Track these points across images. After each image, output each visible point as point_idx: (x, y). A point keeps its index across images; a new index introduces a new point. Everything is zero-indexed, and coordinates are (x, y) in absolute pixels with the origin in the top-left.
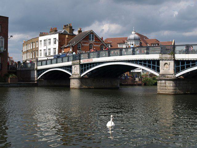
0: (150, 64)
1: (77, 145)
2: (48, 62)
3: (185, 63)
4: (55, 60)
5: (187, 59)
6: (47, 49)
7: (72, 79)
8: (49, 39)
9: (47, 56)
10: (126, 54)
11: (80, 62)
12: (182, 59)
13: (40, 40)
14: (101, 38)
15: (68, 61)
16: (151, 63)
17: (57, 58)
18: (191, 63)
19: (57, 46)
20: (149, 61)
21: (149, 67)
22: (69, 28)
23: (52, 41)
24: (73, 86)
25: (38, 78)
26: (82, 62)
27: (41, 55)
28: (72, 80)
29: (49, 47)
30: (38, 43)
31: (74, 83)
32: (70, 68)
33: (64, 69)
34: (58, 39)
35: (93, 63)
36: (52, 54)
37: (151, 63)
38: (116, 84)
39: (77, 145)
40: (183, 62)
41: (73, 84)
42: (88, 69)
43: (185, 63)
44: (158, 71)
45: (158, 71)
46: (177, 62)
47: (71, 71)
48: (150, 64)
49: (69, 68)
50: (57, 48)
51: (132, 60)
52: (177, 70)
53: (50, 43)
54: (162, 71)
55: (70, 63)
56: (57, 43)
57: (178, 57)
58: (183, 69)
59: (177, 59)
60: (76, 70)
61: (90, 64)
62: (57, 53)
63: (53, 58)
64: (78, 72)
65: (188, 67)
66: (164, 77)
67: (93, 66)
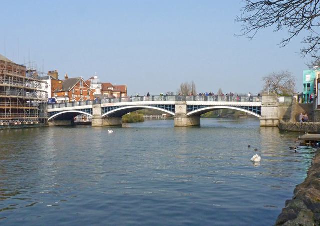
26: (103, 105)
35: (115, 107)
54: (177, 112)
60: (97, 111)
62: (50, 97)
64: (100, 114)
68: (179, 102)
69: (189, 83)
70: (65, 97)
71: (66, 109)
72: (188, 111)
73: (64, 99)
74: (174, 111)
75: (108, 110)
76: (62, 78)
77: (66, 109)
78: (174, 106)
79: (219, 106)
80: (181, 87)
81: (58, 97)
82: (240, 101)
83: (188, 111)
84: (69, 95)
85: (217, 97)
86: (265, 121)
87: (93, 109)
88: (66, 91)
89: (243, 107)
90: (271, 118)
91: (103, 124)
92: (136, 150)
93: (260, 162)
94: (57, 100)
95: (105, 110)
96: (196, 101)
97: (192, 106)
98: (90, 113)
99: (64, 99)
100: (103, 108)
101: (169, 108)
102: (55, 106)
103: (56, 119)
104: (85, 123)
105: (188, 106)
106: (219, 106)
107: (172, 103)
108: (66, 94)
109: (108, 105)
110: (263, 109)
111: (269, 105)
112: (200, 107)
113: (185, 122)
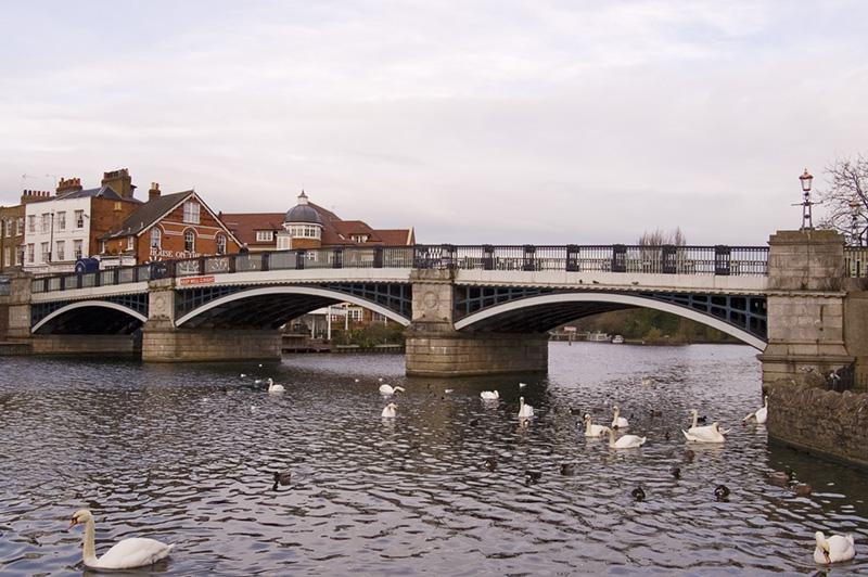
0: (743, 312)
1: (690, 566)
2: (54, 283)
3: (482, 293)
4: (74, 279)
5: (486, 284)
6: (54, 242)
7: (146, 332)
8: (59, 213)
9: (56, 264)
10: (354, 260)
11: (174, 284)
12: (472, 284)
13: (28, 213)
14: (217, 213)
15: (136, 280)
16: (389, 291)
17: (88, 269)
18: (496, 295)
19: (85, 233)
20: (383, 287)
21: (381, 302)
22: (121, 182)
23: (71, 220)
24: (151, 354)
25: (33, 330)
26: (180, 284)
27: (32, 261)
28: (150, 335)
29: (57, 237)
30: (21, 220)
31: (156, 346)
32: (142, 300)
33: (121, 303)
34: (89, 214)
35: (216, 289)
36: (70, 256)
37: (389, 291)
38: (273, 348)
39: (690, 566)
40: (475, 290)
41: (152, 348)
42: (198, 304)
43: (482, 293)
44: (407, 313)
45: (407, 313)
46: (459, 290)
47: (144, 310)
48: (743, 312)
49: (140, 301)
50: (86, 242)
51: (332, 281)
52: (459, 310)
53: (63, 225)
54: (416, 315)
55: (141, 287)
56: (87, 223)
57: (466, 277)
58: (476, 308)
59: (459, 283)
60: (161, 305)
61: (207, 290)
62: (85, 254)
63: (72, 269)
64: (169, 312)
65: (489, 304)
66: (429, 327)
67: (216, 297)
74: (407, 311)
78: (758, 303)
79: (276, 285)
86: (782, 367)
90: (812, 350)
91: (178, 352)
92: (32, 487)
93: (765, 423)
95: (186, 299)
98: (395, 306)
100: (179, 293)
103: (56, 327)
110: (774, 307)
111: (804, 288)
113: (446, 359)
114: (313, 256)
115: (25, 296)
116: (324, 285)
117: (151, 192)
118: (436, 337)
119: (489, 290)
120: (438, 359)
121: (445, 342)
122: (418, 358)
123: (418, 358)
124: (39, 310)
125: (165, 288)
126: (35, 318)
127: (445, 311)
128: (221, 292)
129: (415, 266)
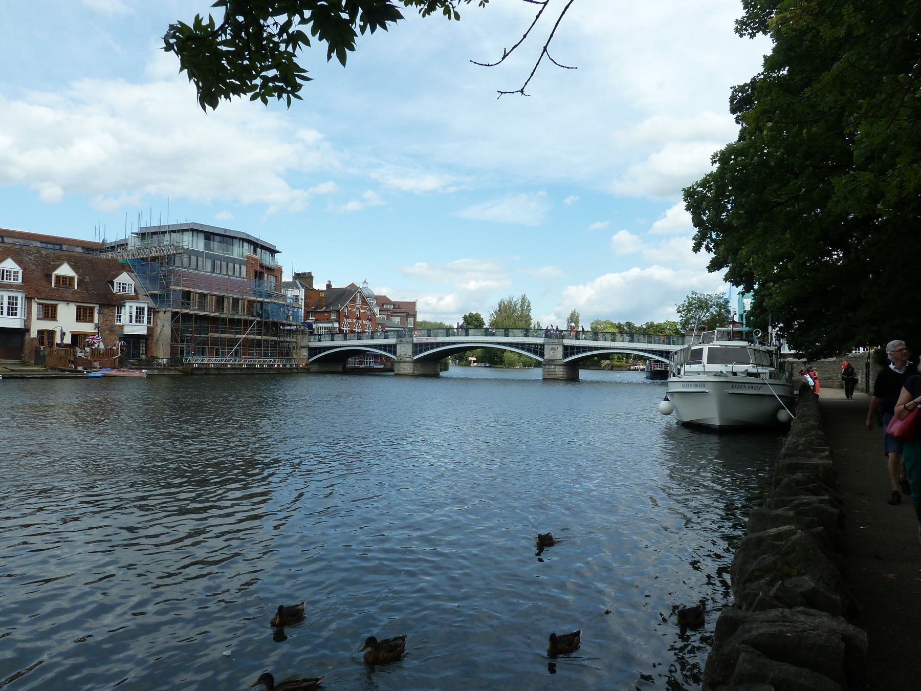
26: (416, 340)
34: (303, 298)
49: (392, 348)
54: (546, 357)
66: (551, 362)
68: (551, 341)
69: (517, 298)
70: (332, 321)
71: (613, 344)
72: (565, 355)
73: (329, 325)
74: (395, 354)
75: (430, 346)
76: (319, 285)
77: (613, 344)
78: (395, 346)
79: (345, 346)
80: (500, 306)
81: (316, 321)
82: (651, 343)
83: (415, 353)
84: (338, 317)
85: (669, 337)
87: (398, 347)
88: (334, 311)
89: (656, 351)
94: (314, 326)
96: (579, 339)
97: (572, 347)
99: (329, 325)
101: (388, 348)
102: (312, 338)
104: (362, 369)
105: (566, 348)
106: (345, 346)
107: (540, 341)
108: (333, 317)
109: (425, 340)
112: (438, 345)
113: (561, 373)
114: (618, 336)
115: (304, 343)
116: (499, 344)
117: (327, 285)
118: (558, 365)
119: (427, 344)
120: (558, 373)
121: (561, 367)
122: (550, 373)
123: (550, 373)
124: (313, 351)
125: (407, 342)
126: (311, 356)
127: (410, 352)
128: (588, 349)
129: (545, 337)
